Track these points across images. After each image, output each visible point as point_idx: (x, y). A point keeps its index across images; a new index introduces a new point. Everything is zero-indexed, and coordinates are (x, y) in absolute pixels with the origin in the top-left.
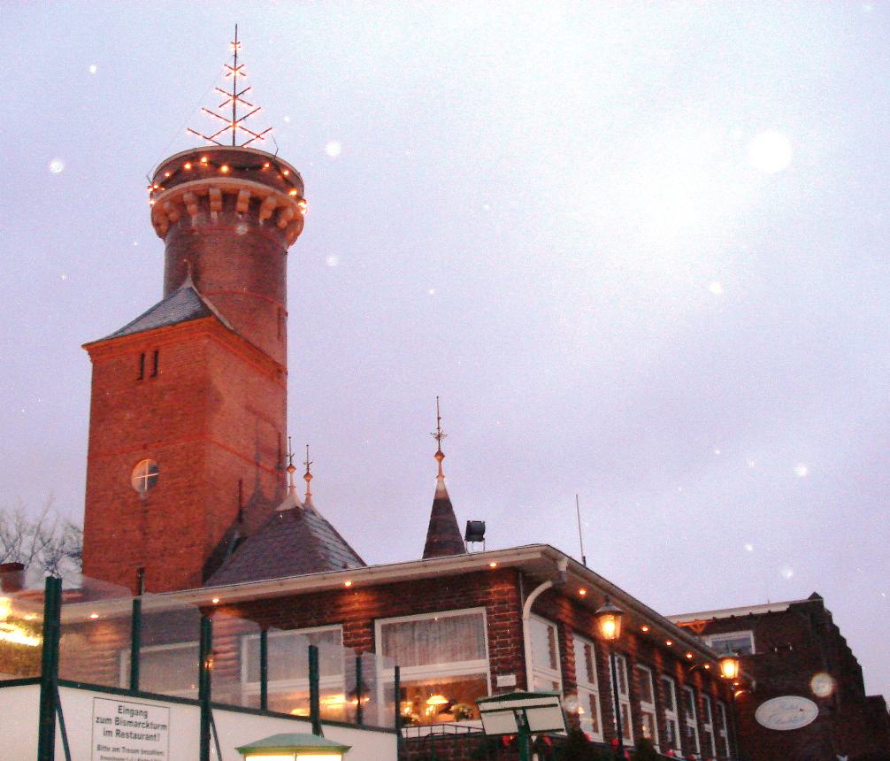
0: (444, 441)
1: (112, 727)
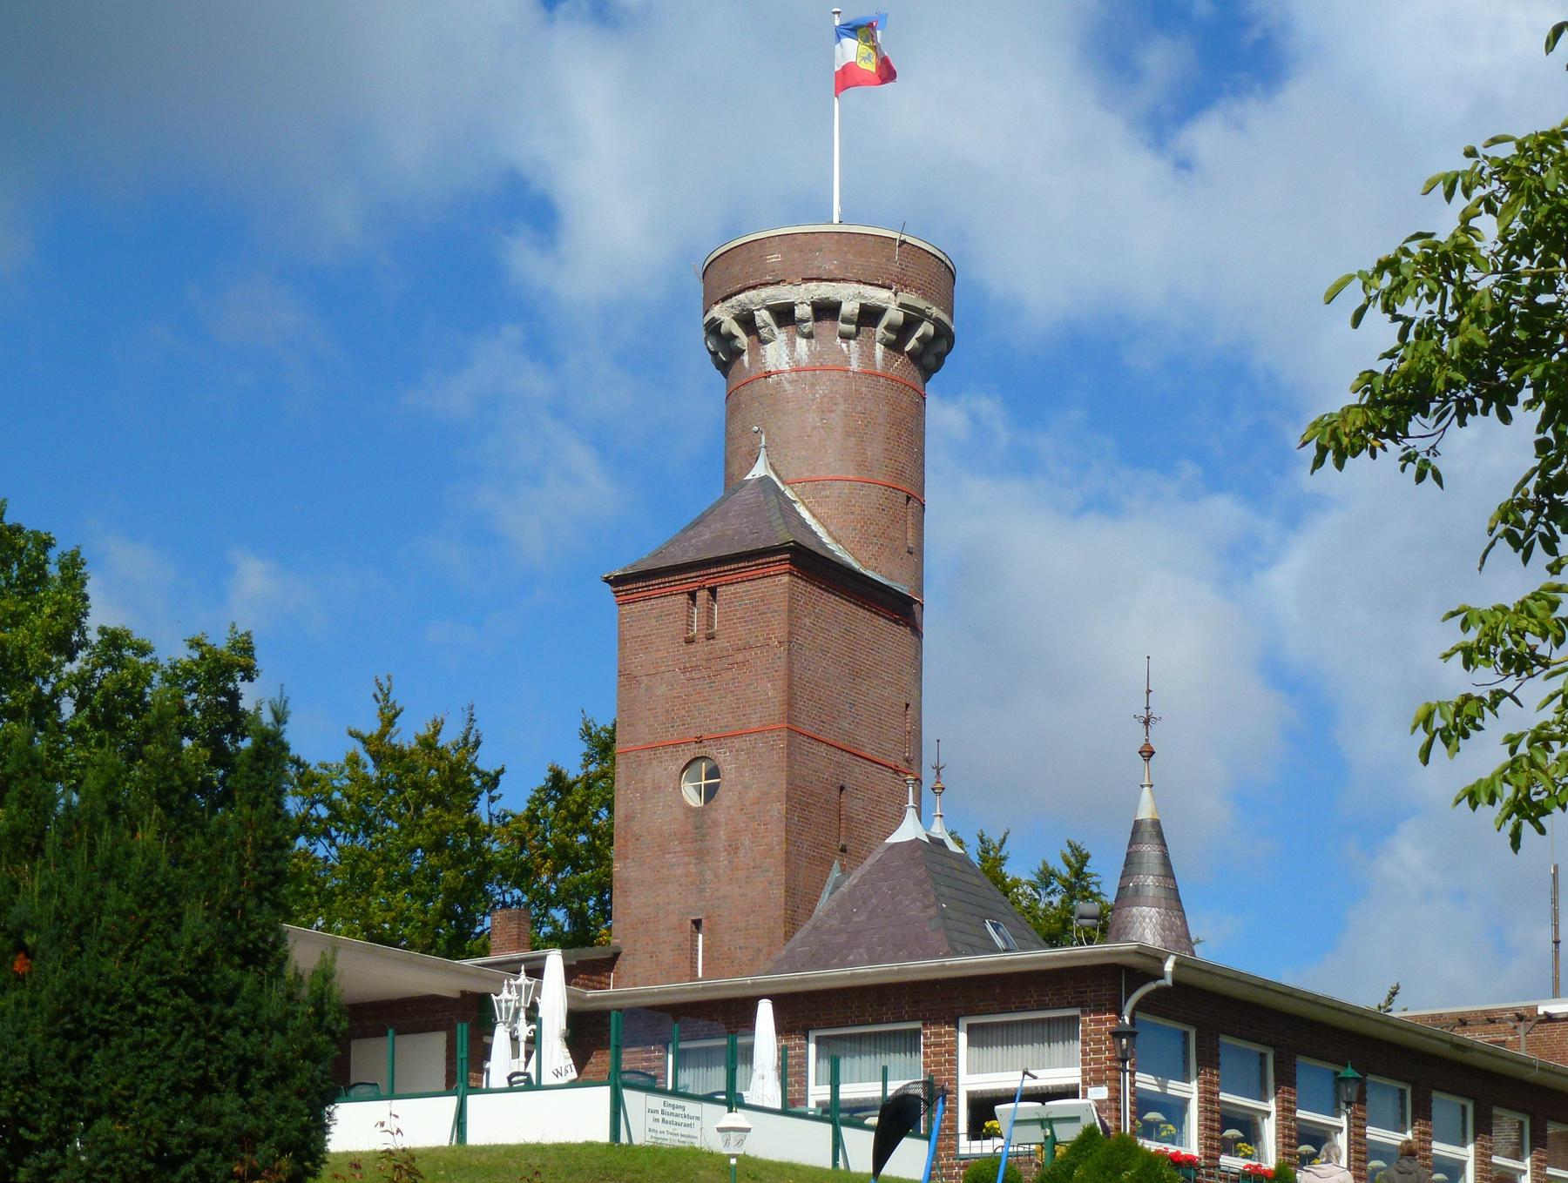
0: (1154, 728)
1: (660, 1116)
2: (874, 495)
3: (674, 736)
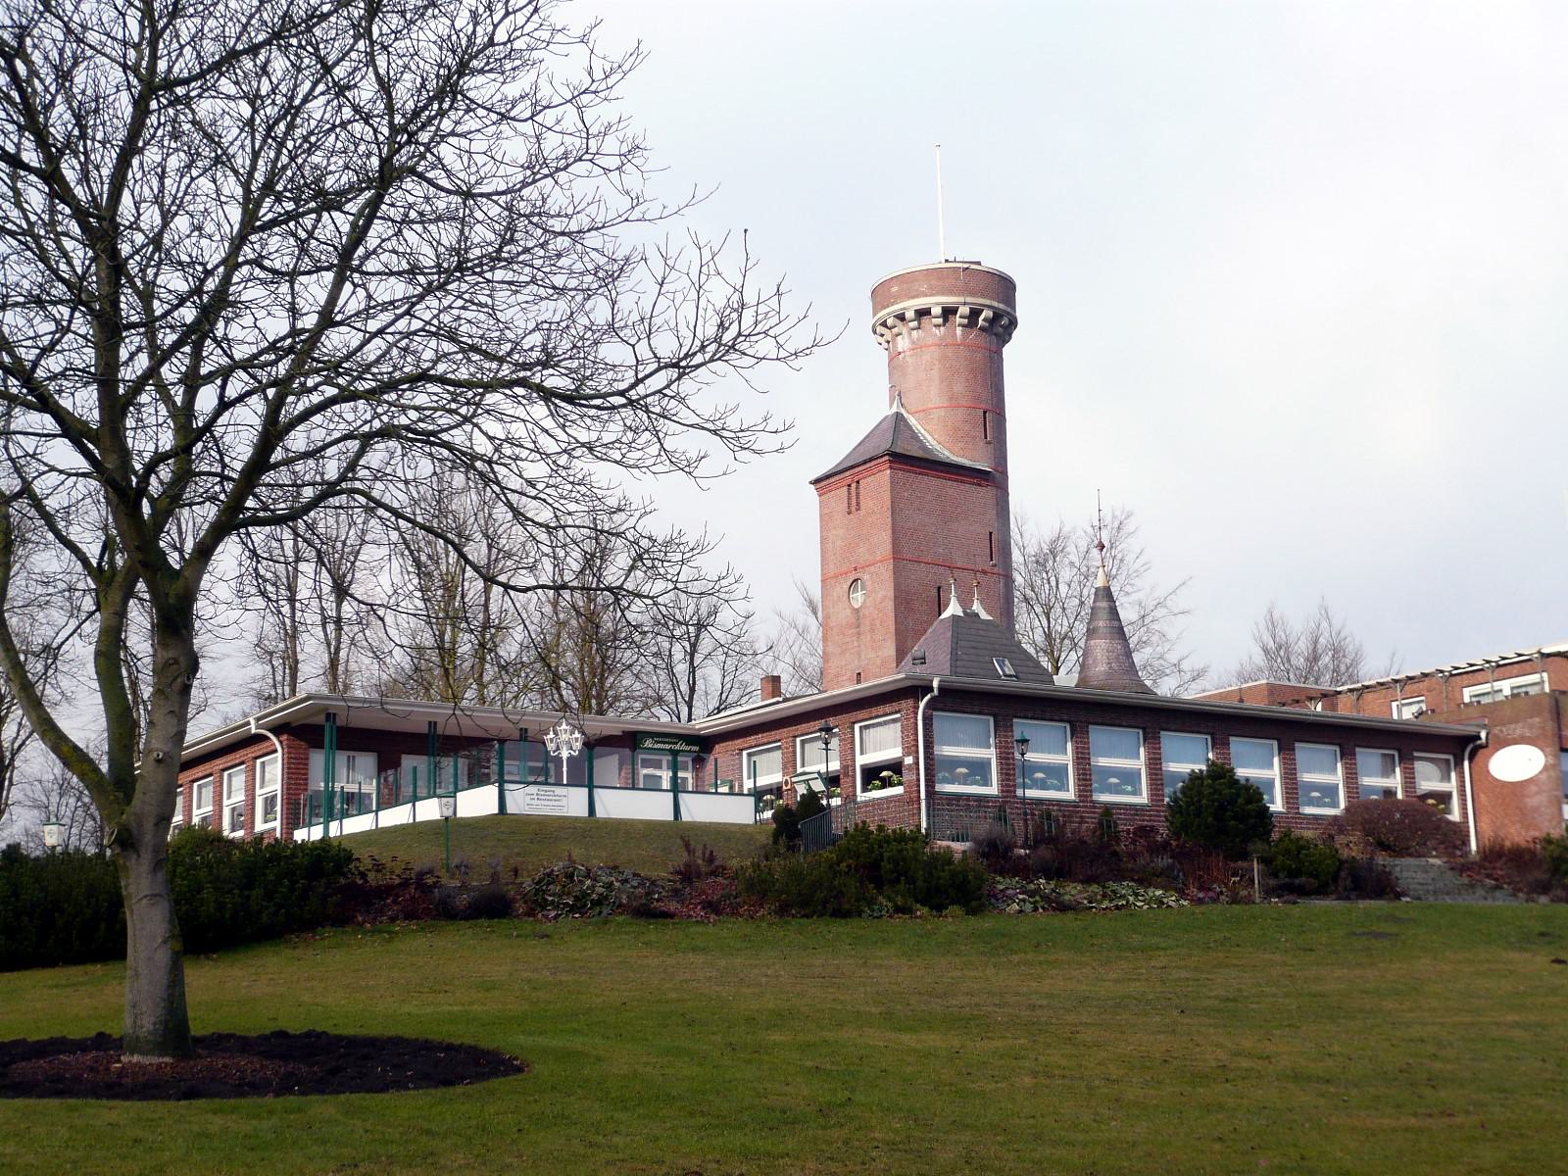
2: (961, 413)
3: (844, 569)
